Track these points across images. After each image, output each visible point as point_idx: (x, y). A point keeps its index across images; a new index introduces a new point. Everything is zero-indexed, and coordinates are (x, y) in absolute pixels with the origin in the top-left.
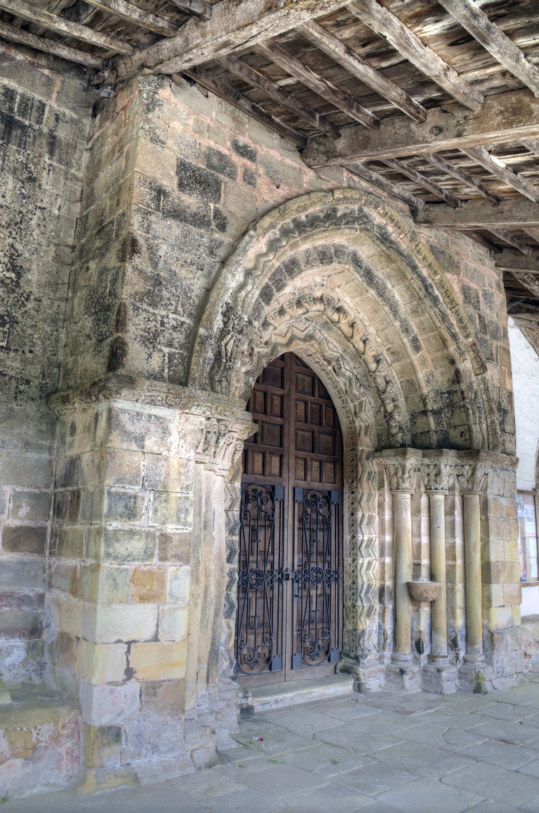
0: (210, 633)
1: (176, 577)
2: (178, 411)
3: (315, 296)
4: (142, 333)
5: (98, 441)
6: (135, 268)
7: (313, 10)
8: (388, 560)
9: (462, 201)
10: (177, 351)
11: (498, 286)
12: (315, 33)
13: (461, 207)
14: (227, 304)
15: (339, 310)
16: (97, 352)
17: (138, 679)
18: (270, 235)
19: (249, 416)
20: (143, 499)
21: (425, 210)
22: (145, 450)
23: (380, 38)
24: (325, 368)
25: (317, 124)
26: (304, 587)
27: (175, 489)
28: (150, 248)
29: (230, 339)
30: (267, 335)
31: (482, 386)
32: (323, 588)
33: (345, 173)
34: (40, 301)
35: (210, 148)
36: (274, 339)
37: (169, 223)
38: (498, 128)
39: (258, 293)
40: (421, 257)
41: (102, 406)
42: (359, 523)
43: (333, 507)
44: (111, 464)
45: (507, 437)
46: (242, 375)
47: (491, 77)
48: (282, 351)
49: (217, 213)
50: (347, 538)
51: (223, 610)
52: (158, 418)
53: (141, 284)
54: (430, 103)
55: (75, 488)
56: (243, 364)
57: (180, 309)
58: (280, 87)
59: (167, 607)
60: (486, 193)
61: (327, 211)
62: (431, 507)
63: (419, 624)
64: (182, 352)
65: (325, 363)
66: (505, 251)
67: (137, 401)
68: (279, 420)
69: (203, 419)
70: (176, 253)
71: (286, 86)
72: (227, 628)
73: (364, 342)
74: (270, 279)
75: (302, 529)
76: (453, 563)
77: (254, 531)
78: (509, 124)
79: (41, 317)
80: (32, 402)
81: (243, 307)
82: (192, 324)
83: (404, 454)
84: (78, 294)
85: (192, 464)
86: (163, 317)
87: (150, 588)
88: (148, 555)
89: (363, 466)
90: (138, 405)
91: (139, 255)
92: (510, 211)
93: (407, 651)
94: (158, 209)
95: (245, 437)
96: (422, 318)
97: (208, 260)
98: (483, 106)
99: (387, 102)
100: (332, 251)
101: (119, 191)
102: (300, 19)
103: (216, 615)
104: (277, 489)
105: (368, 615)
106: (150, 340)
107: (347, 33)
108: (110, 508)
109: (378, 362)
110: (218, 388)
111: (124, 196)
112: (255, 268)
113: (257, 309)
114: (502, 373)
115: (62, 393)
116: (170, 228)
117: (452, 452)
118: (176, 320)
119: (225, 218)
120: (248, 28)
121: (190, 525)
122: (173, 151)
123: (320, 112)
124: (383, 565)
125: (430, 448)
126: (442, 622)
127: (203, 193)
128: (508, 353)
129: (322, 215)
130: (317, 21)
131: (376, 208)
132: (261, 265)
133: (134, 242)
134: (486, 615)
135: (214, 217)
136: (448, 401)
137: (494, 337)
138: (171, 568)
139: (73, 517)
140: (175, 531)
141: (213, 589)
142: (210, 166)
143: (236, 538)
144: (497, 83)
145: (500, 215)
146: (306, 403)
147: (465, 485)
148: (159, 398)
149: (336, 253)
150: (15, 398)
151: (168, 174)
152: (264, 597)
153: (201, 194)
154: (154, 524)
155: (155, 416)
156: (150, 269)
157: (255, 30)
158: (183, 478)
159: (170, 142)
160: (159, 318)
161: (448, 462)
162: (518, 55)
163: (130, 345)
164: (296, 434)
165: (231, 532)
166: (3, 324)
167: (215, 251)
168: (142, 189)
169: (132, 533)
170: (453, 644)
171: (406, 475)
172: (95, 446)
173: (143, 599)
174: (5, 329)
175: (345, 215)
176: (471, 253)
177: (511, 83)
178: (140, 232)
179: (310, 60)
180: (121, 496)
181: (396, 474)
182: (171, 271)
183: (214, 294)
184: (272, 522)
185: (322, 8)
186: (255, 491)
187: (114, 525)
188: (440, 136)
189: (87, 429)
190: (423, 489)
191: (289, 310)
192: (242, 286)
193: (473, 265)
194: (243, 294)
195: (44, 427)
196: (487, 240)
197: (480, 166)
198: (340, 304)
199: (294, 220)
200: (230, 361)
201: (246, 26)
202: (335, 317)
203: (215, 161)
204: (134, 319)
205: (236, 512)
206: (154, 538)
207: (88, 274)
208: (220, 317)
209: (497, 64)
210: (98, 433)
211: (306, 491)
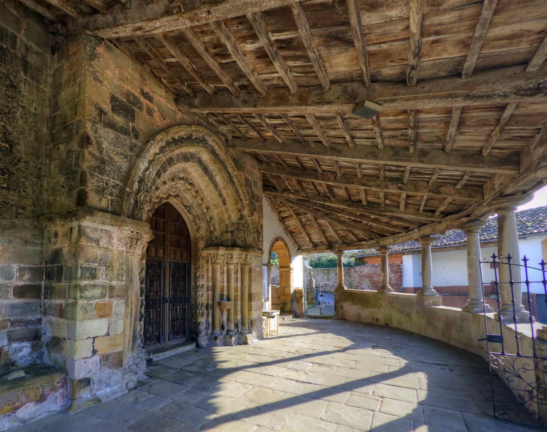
0: (133, 329)
1: (118, 305)
2: (117, 228)
5: (73, 241)
6: (90, 153)
7: (192, 20)
8: (210, 293)
9: (249, 138)
12: (190, 35)
14: (140, 177)
15: (191, 184)
16: (69, 195)
18: (161, 144)
19: (151, 231)
20: (100, 270)
21: (232, 141)
22: (100, 246)
23: (224, 46)
25: (185, 88)
26: (174, 306)
27: (116, 265)
28: (97, 142)
30: (157, 193)
32: (182, 305)
33: (197, 117)
34: (28, 163)
35: (129, 91)
36: (161, 195)
38: (273, 105)
39: (155, 173)
41: (75, 224)
43: (187, 272)
44: (82, 253)
45: (260, 243)
46: (146, 211)
47: (273, 79)
48: (164, 201)
49: (133, 128)
50: (193, 284)
51: (138, 317)
52: (106, 231)
54: (243, 87)
55: (59, 265)
56: (147, 206)
57: (116, 177)
58: (167, 62)
59: (113, 320)
60: (261, 136)
63: (223, 318)
68: (163, 233)
70: (112, 147)
71: (171, 62)
72: (140, 325)
73: (202, 200)
74: (161, 167)
75: (173, 281)
77: (151, 282)
78: (277, 105)
79: (29, 172)
80: (28, 220)
81: (148, 179)
83: (218, 249)
84: (54, 162)
85: (124, 253)
86: (107, 180)
88: (103, 296)
89: (200, 253)
92: (270, 146)
93: (218, 330)
94: (101, 121)
95: (148, 240)
96: (228, 191)
97: (130, 153)
98: (267, 93)
99: (222, 82)
100: (189, 155)
101: (76, 105)
102: (184, 24)
103: (135, 320)
104: (162, 263)
105: (202, 316)
106: (101, 192)
107: (207, 39)
108: (82, 275)
109: (207, 209)
111: (80, 110)
112: (153, 160)
113: (154, 180)
114: (259, 217)
115: (48, 216)
116: (108, 133)
117: (238, 249)
118: (114, 182)
119: (138, 132)
120: (154, 21)
121: (124, 281)
122: (108, 88)
123: (187, 82)
124: (208, 295)
126: (232, 317)
127: (125, 116)
128: (262, 208)
130: (192, 28)
131: (210, 137)
132: (156, 159)
133: (88, 138)
134: (250, 314)
135: (132, 131)
137: (257, 201)
138: (115, 302)
139: (59, 279)
141: (134, 310)
142: (129, 101)
143: (144, 285)
144: (275, 82)
145: (265, 147)
146: (175, 226)
147: (243, 262)
149: (191, 156)
150: (16, 217)
151: (106, 102)
152: (157, 311)
153: (125, 116)
156: (98, 154)
157: (158, 24)
158: (120, 259)
159: (105, 82)
160: (105, 181)
161: (236, 253)
162: (287, 70)
163: (90, 194)
164: (171, 239)
165: (141, 283)
166: (4, 174)
167: (133, 149)
168: (91, 107)
169: (94, 286)
170: (236, 326)
171: (219, 258)
172: (71, 244)
173: (101, 317)
174: (5, 177)
175: (196, 138)
177: (281, 83)
178: (91, 133)
179: (185, 50)
180: (87, 269)
181: (214, 257)
182: (110, 156)
183: (133, 171)
184: (160, 278)
185: (198, 21)
186: (152, 264)
187: (84, 283)
188: (246, 105)
189: (65, 235)
190: (225, 264)
191: (168, 183)
192: (147, 169)
193: (250, 169)
194: (148, 173)
195: (36, 233)
196: (256, 157)
199: (172, 138)
201: (153, 20)
202: (189, 187)
203: (131, 98)
205: (144, 274)
206: (106, 288)
207: (59, 151)
208: (136, 183)
209: (277, 72)
210: (72, 237)
211: (175, 264)
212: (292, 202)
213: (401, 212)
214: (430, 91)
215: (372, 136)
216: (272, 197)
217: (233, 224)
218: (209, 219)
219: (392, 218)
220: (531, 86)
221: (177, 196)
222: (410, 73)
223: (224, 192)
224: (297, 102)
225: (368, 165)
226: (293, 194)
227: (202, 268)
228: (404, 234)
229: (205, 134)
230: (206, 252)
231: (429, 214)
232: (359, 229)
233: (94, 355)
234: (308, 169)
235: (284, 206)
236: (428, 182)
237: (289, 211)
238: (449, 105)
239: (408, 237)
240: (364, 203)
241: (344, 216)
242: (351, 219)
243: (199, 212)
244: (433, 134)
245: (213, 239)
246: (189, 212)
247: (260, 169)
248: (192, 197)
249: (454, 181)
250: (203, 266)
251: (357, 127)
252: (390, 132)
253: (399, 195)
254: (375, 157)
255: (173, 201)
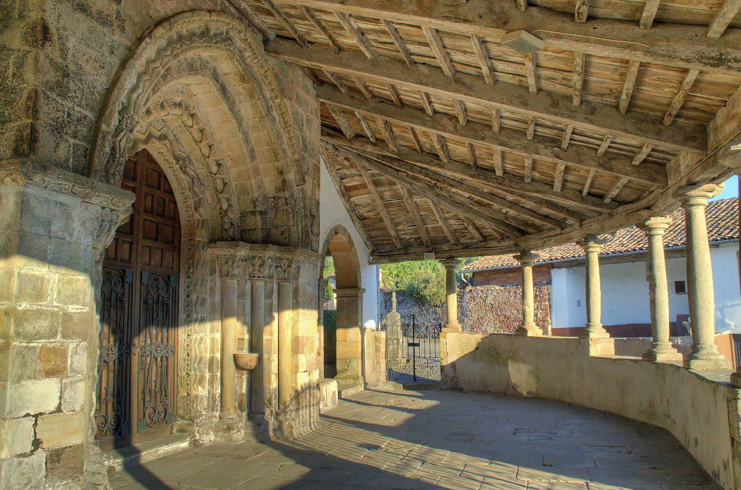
1: (76, 353)
3: (176, 101)
4: (51, 122)
9: (309, 42)
10: (80, 143)
11: (316, 114)
13: (307, 47)
14: (123, 104)
17: (43, 449)
22: (51, 235)
24: (172, 166)
29: (123, 137)
31: (301, 195)
37: (77, 15)
40: (267, 82)
42: (194, 304)
48: (141, 147)
53: (52, 73)
57: (84, 102)
60: (333, 42)
61: (203, 29)
62: (254, 291)
64: (84, 144)
65: (174, 161)
66: (325, 86)
67: (45, 187)
69: (100, 208)
76: (270, 338)
82: (93, 119)
87: (54, 363)
88: (53, 334)
90: (46, 191)
91: (50, 43)
110: (112, 181)
125: (257, 243)
129: (198, 31)
136: (273, 205)
140: (76, 311)
146: (153, 196)
148: (67, 187)
154: (58, 304)
155: (61, 203)
160: (66, 109)
163: (41, 132)
171: (236, 265)
173: (49, 374)
175: (216, 35)
176: (303, 86)
182: (77, 64)
190: (247, 277)
192: (134, 89)
194: (135, 96)
196: (317, 78)
197: (339, 23)
198: (194, 112)
200: (123, 157)
202: (189, 122)
204: (45, 108)
208: (116, 116)
212: (368, 160)
213: (555, 194)
214: (603, 36)
215: (521, 72)
216: (330, 147)
217: (266, 197)
218: (220, 186)
219: (540, 202)
220: (713, 55)
221: (163, 137)
222: (579, 8)
223: (253, 136)
224: (416, 9)
225: (511, 113)
226: (374, 145)
227: (202, 285)
228: (558, 231)
229: (232, 28)
230: (210, 251)
231: (595, 199)
232: (487, 218)
233: (35, 450)
234: (409, 106)
235: (352, 166)
236: (596, 150)
237: (361, 175)
238: (627, 57)
239: (564, 236)
240: (499, 173)
241: (461, 192)
242: (472, 199)
243: (201, 171)
244: (604, 85)
245: (227, 226)
246: (184, 170)
247: (317, 96)
248: (191, 142)
249: (631, 154)
250: (203, 280)
251: (500, 56)
252: (547, 72)
253: (554, 167)
254: (525, 104)
255: (155, 149)
